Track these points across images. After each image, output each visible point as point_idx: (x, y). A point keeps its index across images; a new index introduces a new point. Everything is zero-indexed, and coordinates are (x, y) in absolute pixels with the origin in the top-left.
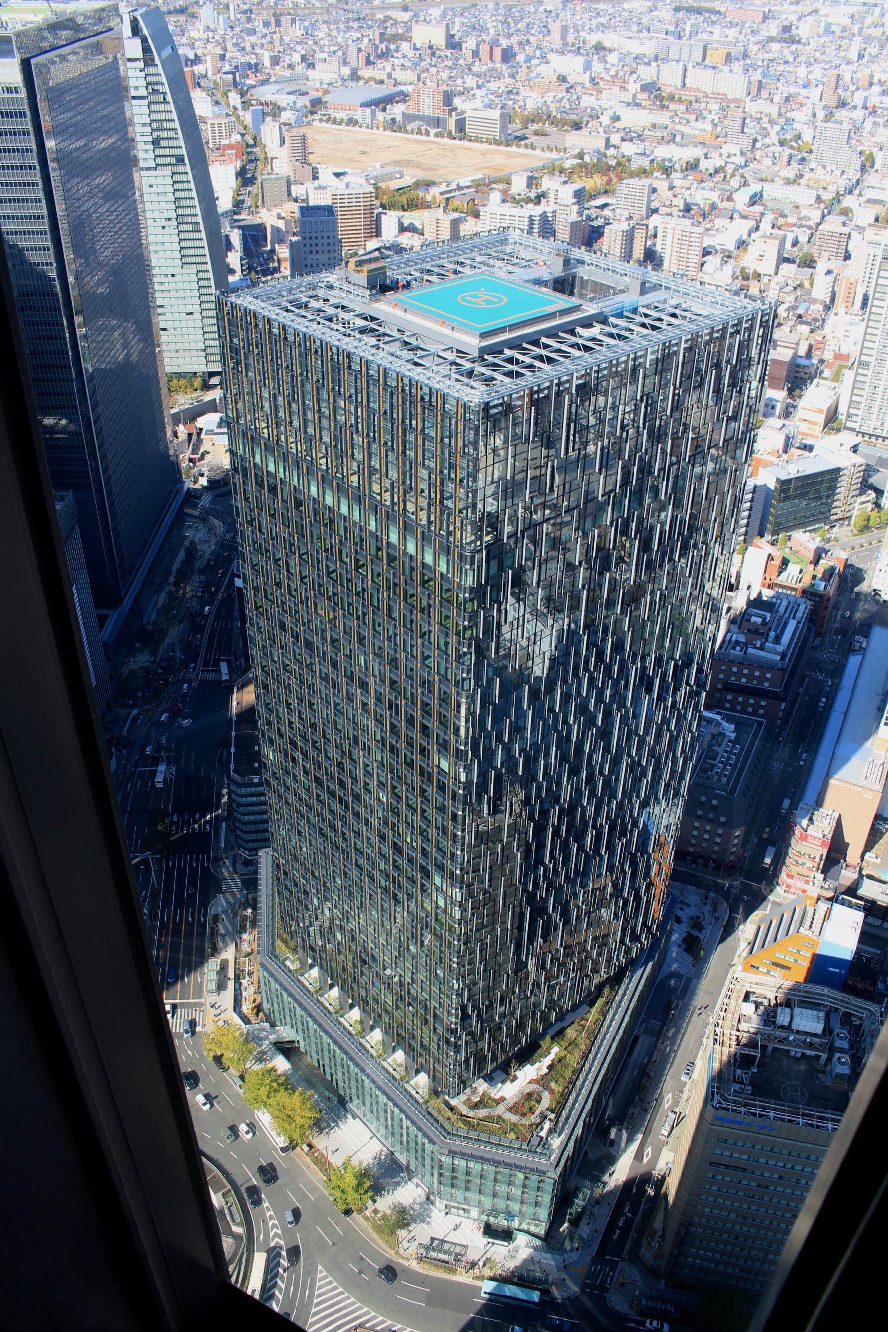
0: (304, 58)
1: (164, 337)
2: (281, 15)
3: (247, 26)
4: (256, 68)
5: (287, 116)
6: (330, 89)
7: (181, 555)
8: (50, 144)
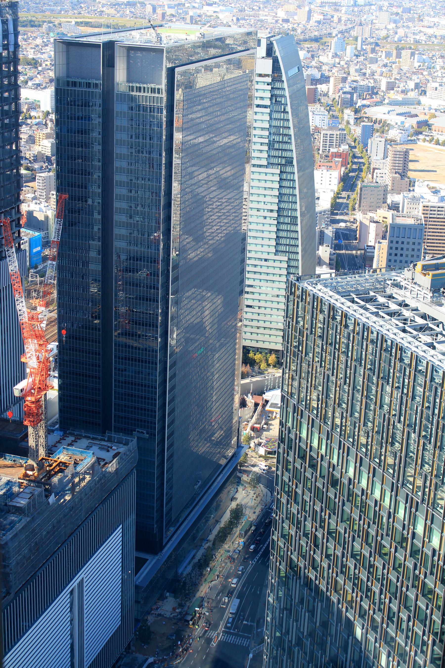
0: (417, 86)
1: (247, 314)
2: (403, 49)
3: (371, 55)
4: (373, 91)
5: (393, 134)
6: (437, 114)
7: (227, 516)
8: (178, 137)
